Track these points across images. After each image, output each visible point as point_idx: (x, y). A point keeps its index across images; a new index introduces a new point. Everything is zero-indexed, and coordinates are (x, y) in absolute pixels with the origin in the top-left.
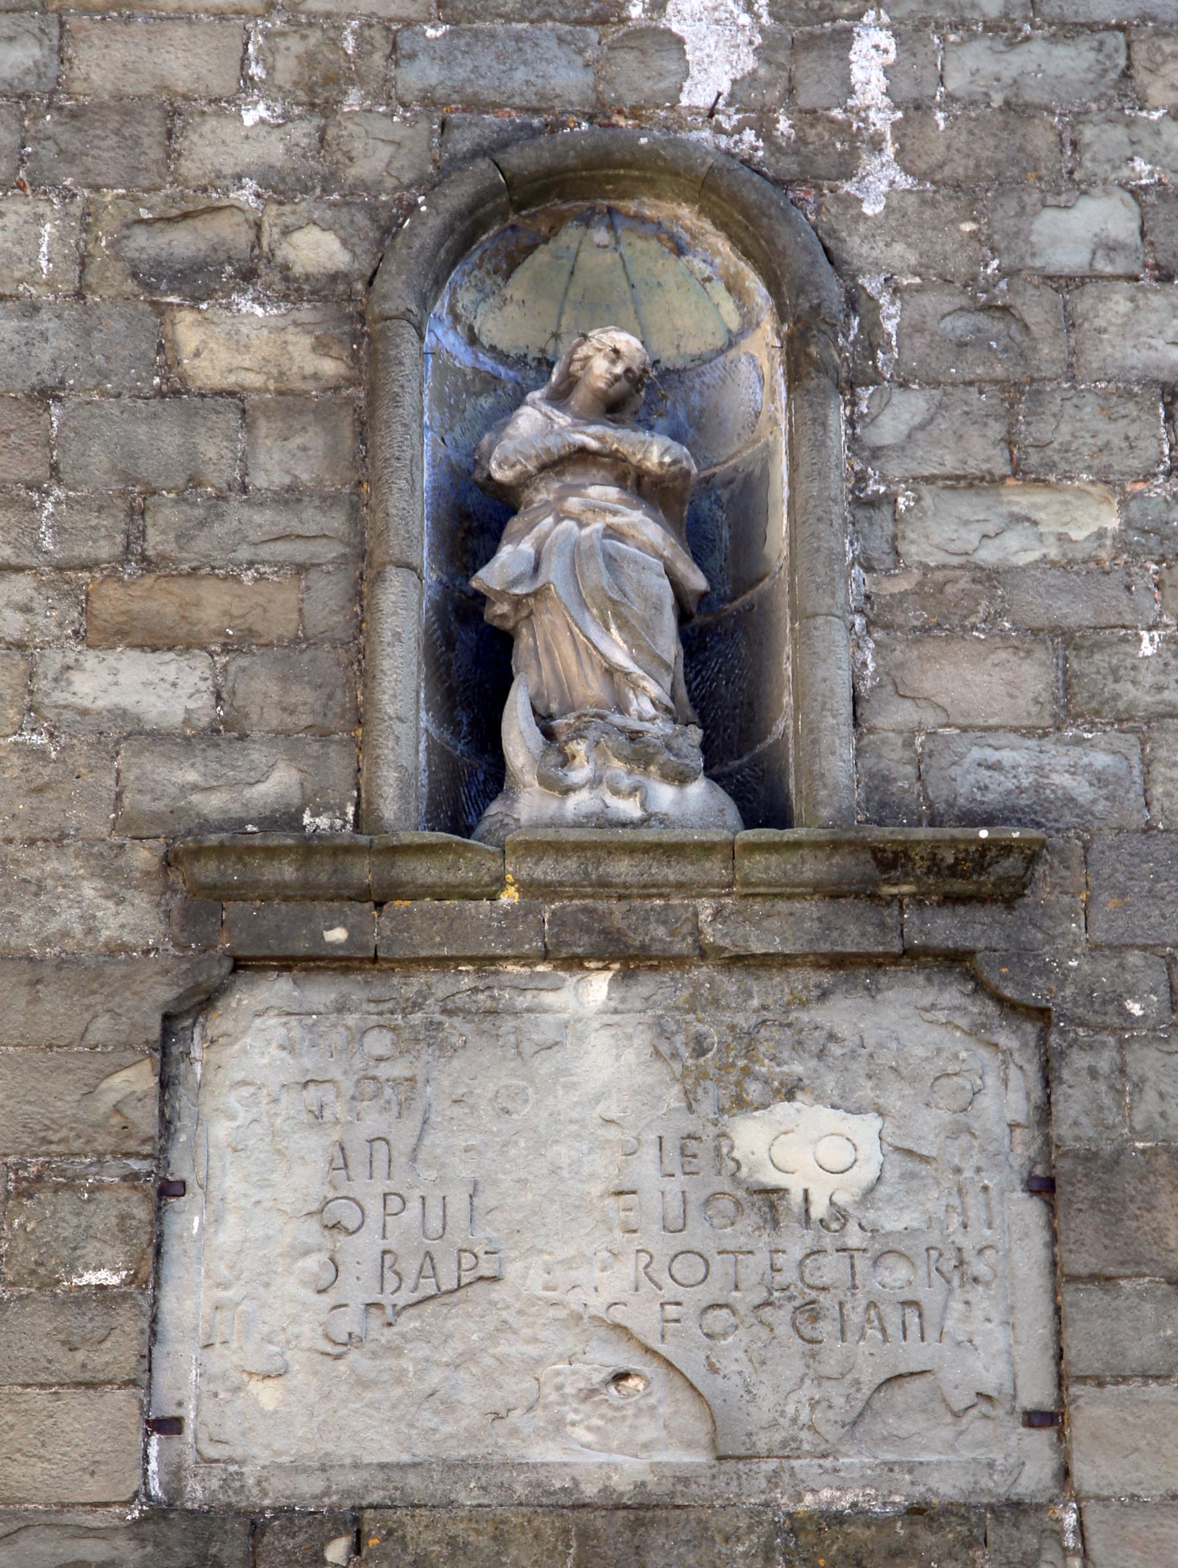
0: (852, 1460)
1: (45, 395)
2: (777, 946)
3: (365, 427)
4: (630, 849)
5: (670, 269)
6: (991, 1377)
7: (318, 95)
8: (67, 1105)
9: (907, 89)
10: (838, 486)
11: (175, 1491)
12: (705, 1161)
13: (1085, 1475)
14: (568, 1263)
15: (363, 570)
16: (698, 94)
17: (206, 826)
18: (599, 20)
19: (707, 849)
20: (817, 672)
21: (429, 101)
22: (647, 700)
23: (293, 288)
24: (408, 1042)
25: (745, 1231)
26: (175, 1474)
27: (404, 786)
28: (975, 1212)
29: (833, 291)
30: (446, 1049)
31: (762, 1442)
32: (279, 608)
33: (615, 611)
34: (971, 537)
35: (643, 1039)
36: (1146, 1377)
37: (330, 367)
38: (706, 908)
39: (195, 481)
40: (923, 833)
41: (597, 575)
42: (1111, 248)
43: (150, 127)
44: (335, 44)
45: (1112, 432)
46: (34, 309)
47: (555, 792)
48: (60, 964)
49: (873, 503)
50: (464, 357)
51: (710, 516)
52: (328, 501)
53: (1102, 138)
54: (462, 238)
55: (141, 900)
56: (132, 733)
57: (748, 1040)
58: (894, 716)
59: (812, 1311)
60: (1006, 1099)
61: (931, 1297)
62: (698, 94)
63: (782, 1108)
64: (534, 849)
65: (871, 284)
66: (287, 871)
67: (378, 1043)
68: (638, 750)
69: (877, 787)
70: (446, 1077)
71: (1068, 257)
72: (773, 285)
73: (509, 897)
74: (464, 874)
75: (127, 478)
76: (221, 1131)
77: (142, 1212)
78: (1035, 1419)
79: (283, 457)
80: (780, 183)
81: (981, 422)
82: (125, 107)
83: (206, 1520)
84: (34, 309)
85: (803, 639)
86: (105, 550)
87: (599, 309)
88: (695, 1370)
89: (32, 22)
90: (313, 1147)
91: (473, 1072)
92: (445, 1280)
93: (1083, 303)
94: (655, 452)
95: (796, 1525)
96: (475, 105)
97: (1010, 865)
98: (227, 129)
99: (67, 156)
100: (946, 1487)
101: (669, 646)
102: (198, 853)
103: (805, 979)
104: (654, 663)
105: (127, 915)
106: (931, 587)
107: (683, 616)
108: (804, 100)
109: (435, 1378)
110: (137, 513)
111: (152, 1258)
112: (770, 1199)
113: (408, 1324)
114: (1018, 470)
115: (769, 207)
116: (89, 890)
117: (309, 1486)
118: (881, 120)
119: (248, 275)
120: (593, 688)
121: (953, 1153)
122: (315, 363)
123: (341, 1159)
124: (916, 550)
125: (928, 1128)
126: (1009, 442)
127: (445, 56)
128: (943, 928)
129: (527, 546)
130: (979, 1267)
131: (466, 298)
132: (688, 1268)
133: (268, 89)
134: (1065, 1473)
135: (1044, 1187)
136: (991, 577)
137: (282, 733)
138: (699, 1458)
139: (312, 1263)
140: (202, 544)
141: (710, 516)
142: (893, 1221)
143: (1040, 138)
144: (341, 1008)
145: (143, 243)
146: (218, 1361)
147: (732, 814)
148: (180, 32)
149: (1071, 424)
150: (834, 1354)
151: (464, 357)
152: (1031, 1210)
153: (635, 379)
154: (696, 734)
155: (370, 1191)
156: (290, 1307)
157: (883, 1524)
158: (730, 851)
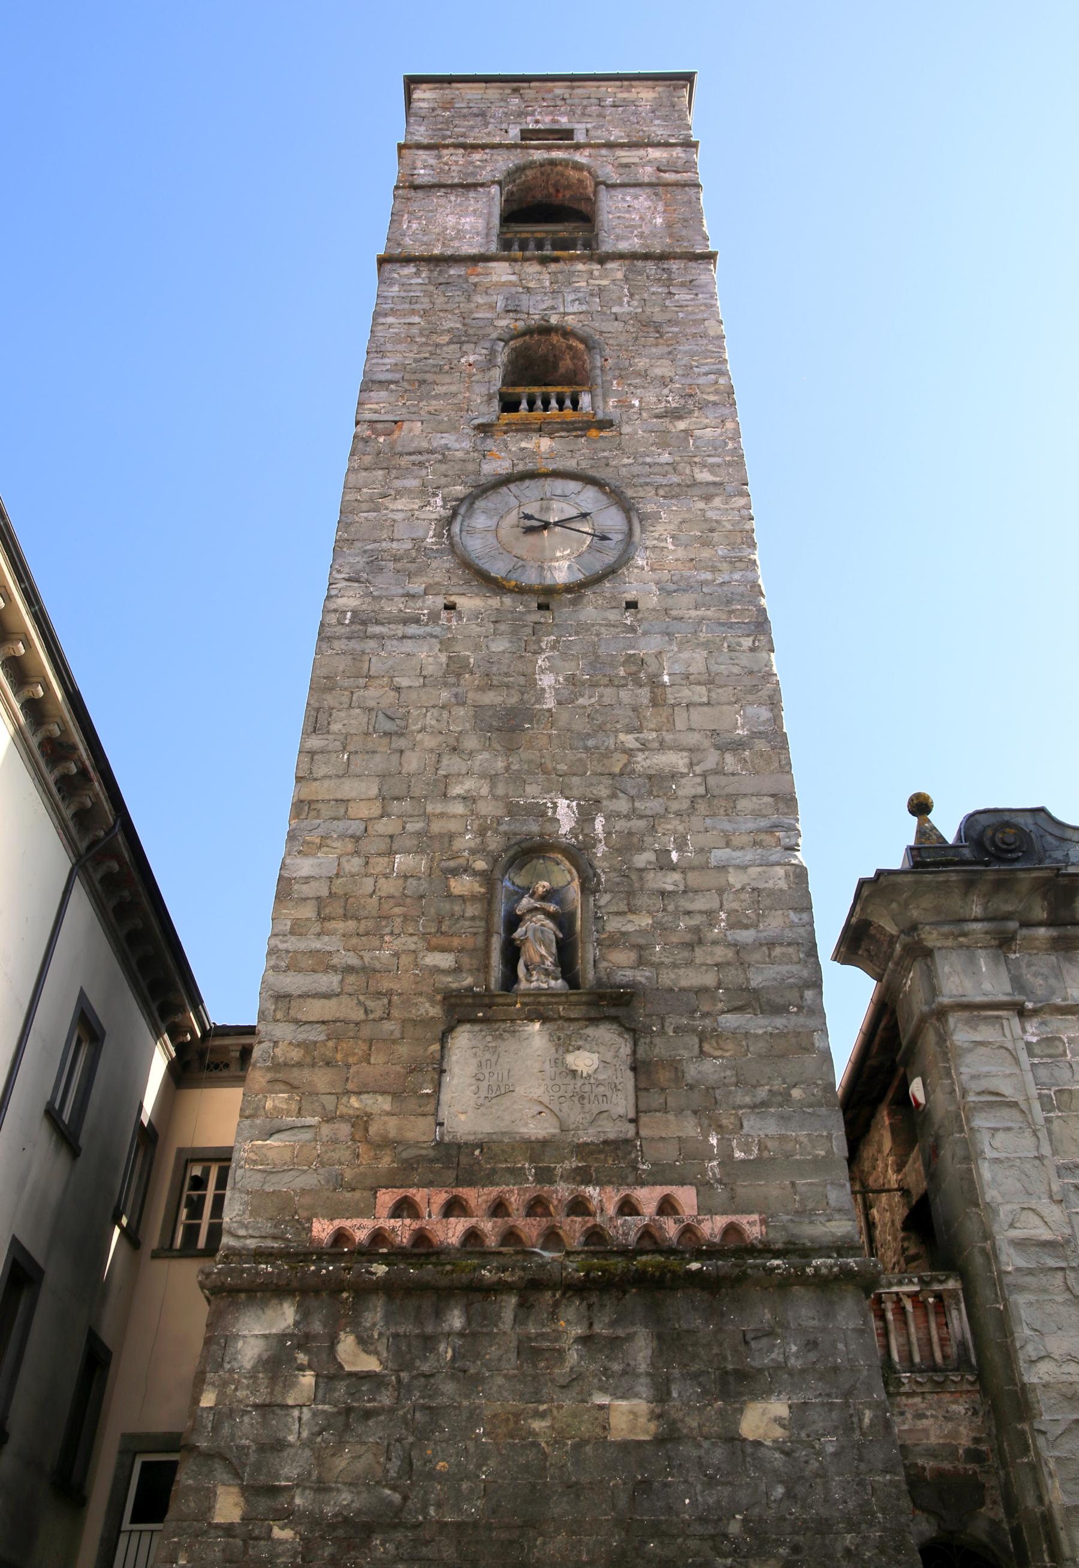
0: (591, 1131)
1: (422, 897)
2: (576, 1016)
3: (490, 903)
4: (545, 995)
5: (556, 868)
6: (622, 1112)
7: (482, 832)
8: (421, 1052)
9: (607, 830)
10: (591, 914)
11: (442, 1138)
12: (560, 1064)
13: (642, 1133)
14: (530, 1087)
15: (488, 934)
16: (562, 831)
17: (453, 990)
18: (542, 816)
19: (561, 995)
20: (587, 953)
21: (505, 833)
22: (549, 962)
23: (475, 873)
24: (495, 1038)
25: (568, 1080)
26: (442, 1135)
27: (496, 981)
28: (619, 1075)
29: (591, 872)
30: (503, 1040)
31: (571, 1127)
32: (470, 942)
33: (543, 942)
34: (619, 926)
35: (547, 1037)
36: (656, 1111)
37: (482, 890)
38: (561, 1008)
39: (453, 915)
40: (609, 990)
41: (539, 934)
42: (650, 863)
43: (446, 839)
44: (486, 822)
45: (650, 902)
46: (420, 878)
47: (530, 982)
48: (421, 1021)
49: (599, 918)
50: (511, 888)
51: (564, 921)
52: (481, 919)
53: (648, 840)
54: (511, 862)
55: (438, 1007)
56: (437, 970)
57: (569, 1037)
58: (603, 965)
59: (583, 1097)
60: (626, 1049)
61: (608, 1094)
62: (562, 831)
63: (577, 1052)
64: (524, 995)
65: (599, 871)
66: (470, 1001)
67: (489, 1038)
68: (547, 973)
69: (599, 980)
70: (503, 1046)
71: (641, 865)
72: (578, 872)
73: (518, 1006)
74: (508, 1001)
75: (439, 915)
76: (454, 1058)
77: (436, 1077)
78: (631, 1121)
79: (471, 910)
80: (580, 850)
81: (621, 900)
82: (441, 836)
83: (449, 1145)
84: (420, 878)
85: (583, 948)
86: (433, 930)
87: (541, 877)
88: (557, 1111)
89: (422, 818)
90: (474, 1062)
91: (509, 1045)
92: (502, 1091)
93: (644, 875)
94: (552, 908)
95: (579, 1146)
96: (515, 834)
97: (627, 997)
98: (462, 840)
99: (428, 846)
100: (612, 1136)
101: (554, 950)
102: (451, 996)
103: (583, 1023)
104: (551, 954)
105: (435, 1010)
106: (611, 936)
107: (557, 943)
108: (585, 832)
109: (499, 1113)
110: (440, 922)
111: (438, 1087)
112: (574, 1073)
113: (494, 1101)
114: (630, 911)
115: (577, 855)
116: (427, 1005)
117: (471, 1138)
118: (601, 836)
119: (465, 871)
120: (537, 959)
121: (614, 1061)
122: (479, 889)
123: (480, 1065)
124: (608, 928)
125: (609, 1056)
126: (628, 904)
127: (509, 823)
128: (613, 1011)
129: (524, 928)
130: (619, 1087)
131: (512, 875)
132: (556, 1088)
133: (471, 831)
134: (637, 1133)
135: (634, 1069)
136: (624, 934)
137: (470, 970)
138: (557, 1131)
139: (473, 1088)
140: (453, 929)
141: (564, 921)
142: (601, 1077)
143: (635, 840)
144: (481, 1031)
145: (444, 864)
146: (453, 1110)
147: (567, 987)
148: (453, 820)
149: (642, 901)
150: (587, 1107)
151: (511, 888)
152: (630, 1075)
153: (548, 892)
154: (560, 969)
155: (486, 1072)
156: (468, 1097)
157: (597, 1145)
158: (566, 995)
